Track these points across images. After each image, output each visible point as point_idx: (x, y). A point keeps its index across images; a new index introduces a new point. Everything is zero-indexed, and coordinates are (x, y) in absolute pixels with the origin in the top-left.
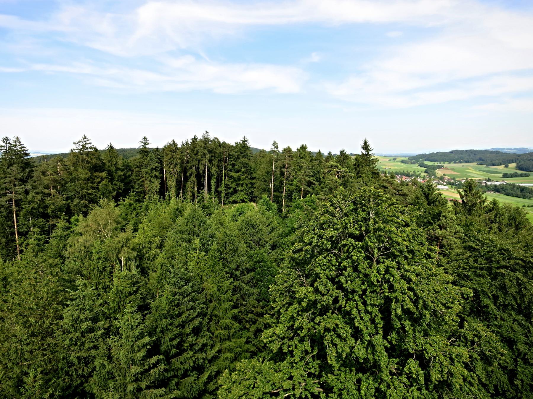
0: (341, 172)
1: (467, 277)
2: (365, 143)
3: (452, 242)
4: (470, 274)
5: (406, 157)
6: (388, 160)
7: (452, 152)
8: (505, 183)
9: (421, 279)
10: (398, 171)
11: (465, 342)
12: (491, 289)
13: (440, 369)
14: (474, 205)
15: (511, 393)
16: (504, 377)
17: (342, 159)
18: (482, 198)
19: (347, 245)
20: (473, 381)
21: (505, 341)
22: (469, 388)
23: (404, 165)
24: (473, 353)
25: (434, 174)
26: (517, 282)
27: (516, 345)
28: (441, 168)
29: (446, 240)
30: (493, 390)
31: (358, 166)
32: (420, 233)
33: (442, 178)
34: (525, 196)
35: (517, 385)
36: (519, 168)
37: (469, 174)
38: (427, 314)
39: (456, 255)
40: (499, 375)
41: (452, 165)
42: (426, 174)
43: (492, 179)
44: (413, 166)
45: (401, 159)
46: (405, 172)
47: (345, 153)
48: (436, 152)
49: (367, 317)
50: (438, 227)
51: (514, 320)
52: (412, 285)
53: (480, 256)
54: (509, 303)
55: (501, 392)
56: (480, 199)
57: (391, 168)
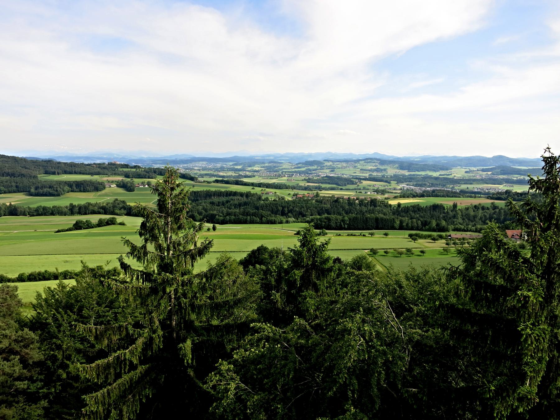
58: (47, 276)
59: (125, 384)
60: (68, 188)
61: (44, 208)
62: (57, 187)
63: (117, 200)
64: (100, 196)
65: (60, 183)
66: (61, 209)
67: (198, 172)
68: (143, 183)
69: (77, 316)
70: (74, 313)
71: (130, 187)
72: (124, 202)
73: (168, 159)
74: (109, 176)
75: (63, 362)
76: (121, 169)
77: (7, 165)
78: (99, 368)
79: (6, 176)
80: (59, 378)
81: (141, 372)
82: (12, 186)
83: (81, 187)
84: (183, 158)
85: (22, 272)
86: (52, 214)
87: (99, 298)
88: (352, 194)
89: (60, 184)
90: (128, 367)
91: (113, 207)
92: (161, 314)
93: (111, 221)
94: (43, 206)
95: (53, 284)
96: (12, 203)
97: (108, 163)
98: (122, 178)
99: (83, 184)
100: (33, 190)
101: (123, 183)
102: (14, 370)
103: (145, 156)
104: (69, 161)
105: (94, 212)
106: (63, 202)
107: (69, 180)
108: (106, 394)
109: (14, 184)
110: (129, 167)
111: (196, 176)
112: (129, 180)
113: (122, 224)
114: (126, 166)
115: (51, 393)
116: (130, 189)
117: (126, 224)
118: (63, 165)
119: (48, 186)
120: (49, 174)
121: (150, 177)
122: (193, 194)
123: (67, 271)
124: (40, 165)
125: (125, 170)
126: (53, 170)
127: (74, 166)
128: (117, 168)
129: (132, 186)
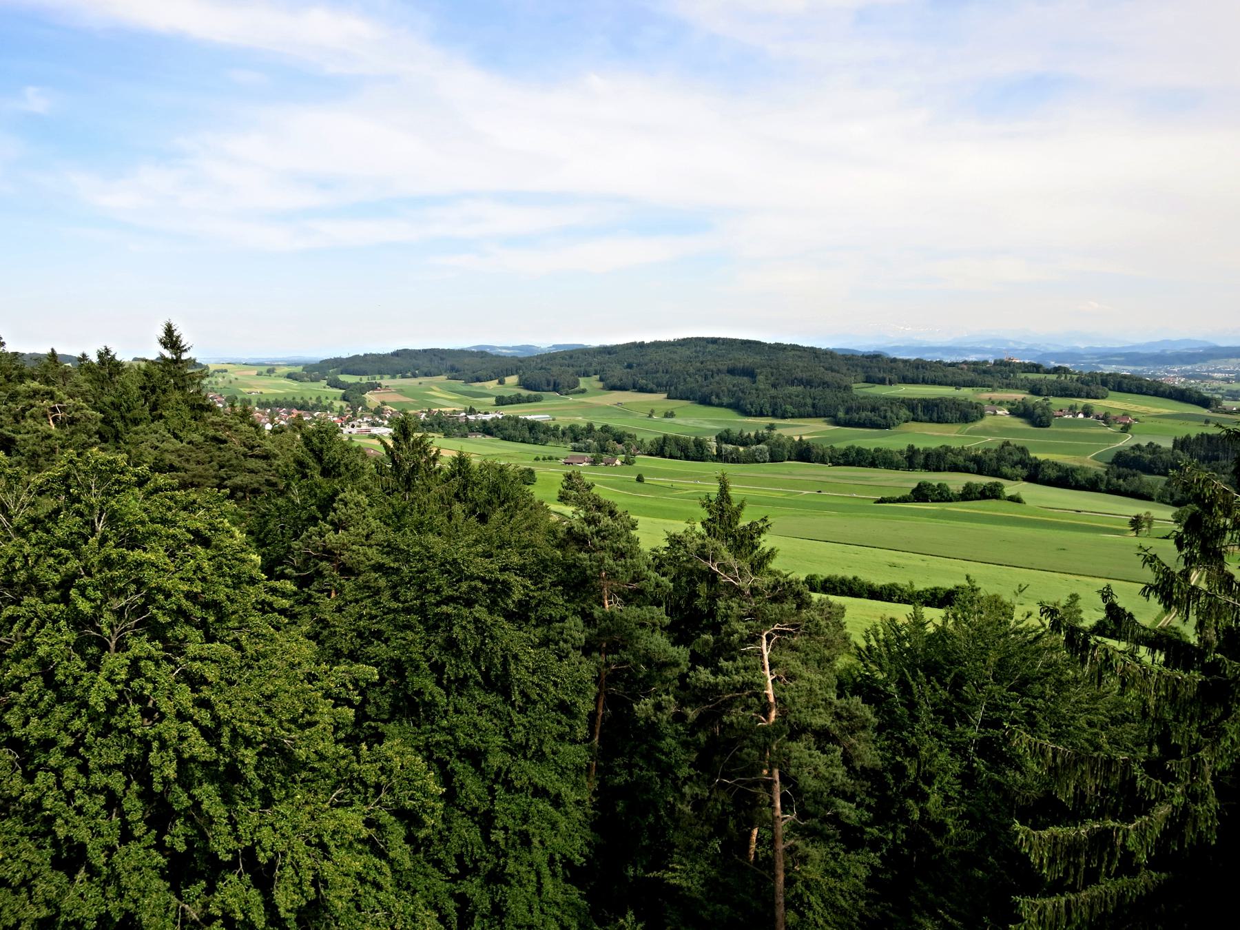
0: (63, 409)
1: (378, 635)
2: (169, 331)
3: (362, 558)
4: (383, 627)
5: (297, 365)
6: (256, 372)
7: (397, 354)
8: (500, 417)
9: (228, 673)
10: (280, 399)
11: (363, 791)
12: (427, 652)
13: (297, 880)
14: (415, 469)
15: (488, 862)
16: (473, 833)
17: (106, 372)
18: (431, 451)
19: (19, 617)
20: (379, 878)
21: (464, 756)
22: (375, 897)
23: (295, 384)
24: (382, 813)
25: (362, 403)
26: (477, 628)
27: (486, 760)
28: (376, 389)
29: (347, 554)
30: (456, 867)
31: (153, 391)
32: (239, 555)
33: (379, 412)
34: (537, 439)
35: (497, 842)
36: (525, 384)
37: (433, 401)
38: (249, 756)
39: (356, 590)
40: (464, 830)
41: (399, 382)
42: (344, 404)
43: (477, 409)
44: (314, 386)
45: (287, 370)
46: (298, 400)
47: (113, 357)
48: (362, 354)
49: (95, 804)
50: (331, 527)
51: (481, 707)
52: (206, 692)
53: (402, 582)
54: (465, 674)
55: (471, 866)
56: (426, 454)
57: (265, 391)
58: (856, 588)
59: (1106, 902)
60: (908, 413)
61: (860, 452)
62: (886, 410)
63: (1007, 444)
64: (969, 432)
65: (892, 401)
66: (889, 455)
67: (1222, 384)
68: (1072, 409)
69: (950, 692)
70: (944, 685)
71: (1039, 416)
72: (1023, 450)
73: (1141, 351)
74: (994, 391)
75: (915, 786)
76: (1023, 376)
77: (800, 364)
78: (1055, 845)
79: (797, 385)
80: (904, 813)
81: (1146, 886)
82: (805, 404)
83: (933, 411)
84: (1181, 348)
85: (813, 573)
86: (873, 464)
87: (998, 665)
89: (892, 403)
90: (1116, 864)
91: (997, 459)
92: (1221, 757)
93: (991, 490)
94: (857, 446)
95: (901, 613)
96: (804, 438)
97: (995, 361)
98: (1023, 396)
99: (937, 405)
100: (841, 414)
101: (1025, 406)
102: (835, 775)
103: (1082, 345)
104: (913, 357)
105: (955, 468)
106: (894, 441)
107: (910, 397)
108: (1063, 910)
109: (809, 401)
110: (1041, 370)
111: (1217, 396)
112: (1039, 399)
113: (1016, 499)
114: (1036, 368)
115: (885, 841)
116: (1041, 421)
117: (1024, 500)
118: (901, 365)
119: (869, 407)
120: (874, 382)
121: (1092, 394)
122: (1205, 442)
123: (894, 585)
124: (857, 365)
125: (1032, 376)
126: (881, 375)
127: (923, 368)
128: (1013, 372)
129: (1044, 414)
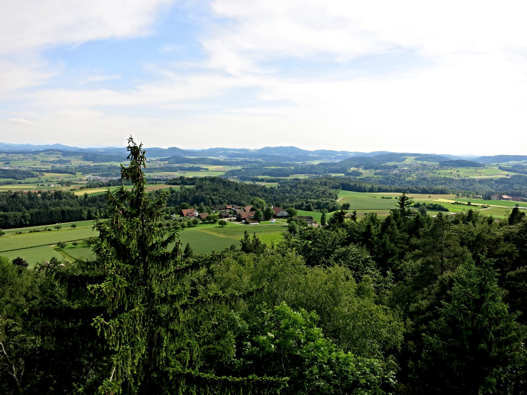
88: (33, 188)
